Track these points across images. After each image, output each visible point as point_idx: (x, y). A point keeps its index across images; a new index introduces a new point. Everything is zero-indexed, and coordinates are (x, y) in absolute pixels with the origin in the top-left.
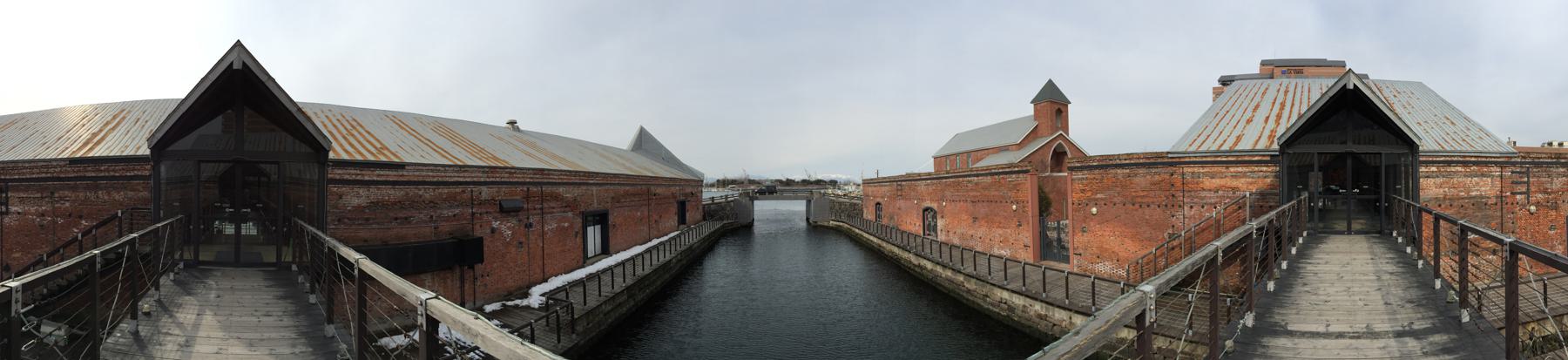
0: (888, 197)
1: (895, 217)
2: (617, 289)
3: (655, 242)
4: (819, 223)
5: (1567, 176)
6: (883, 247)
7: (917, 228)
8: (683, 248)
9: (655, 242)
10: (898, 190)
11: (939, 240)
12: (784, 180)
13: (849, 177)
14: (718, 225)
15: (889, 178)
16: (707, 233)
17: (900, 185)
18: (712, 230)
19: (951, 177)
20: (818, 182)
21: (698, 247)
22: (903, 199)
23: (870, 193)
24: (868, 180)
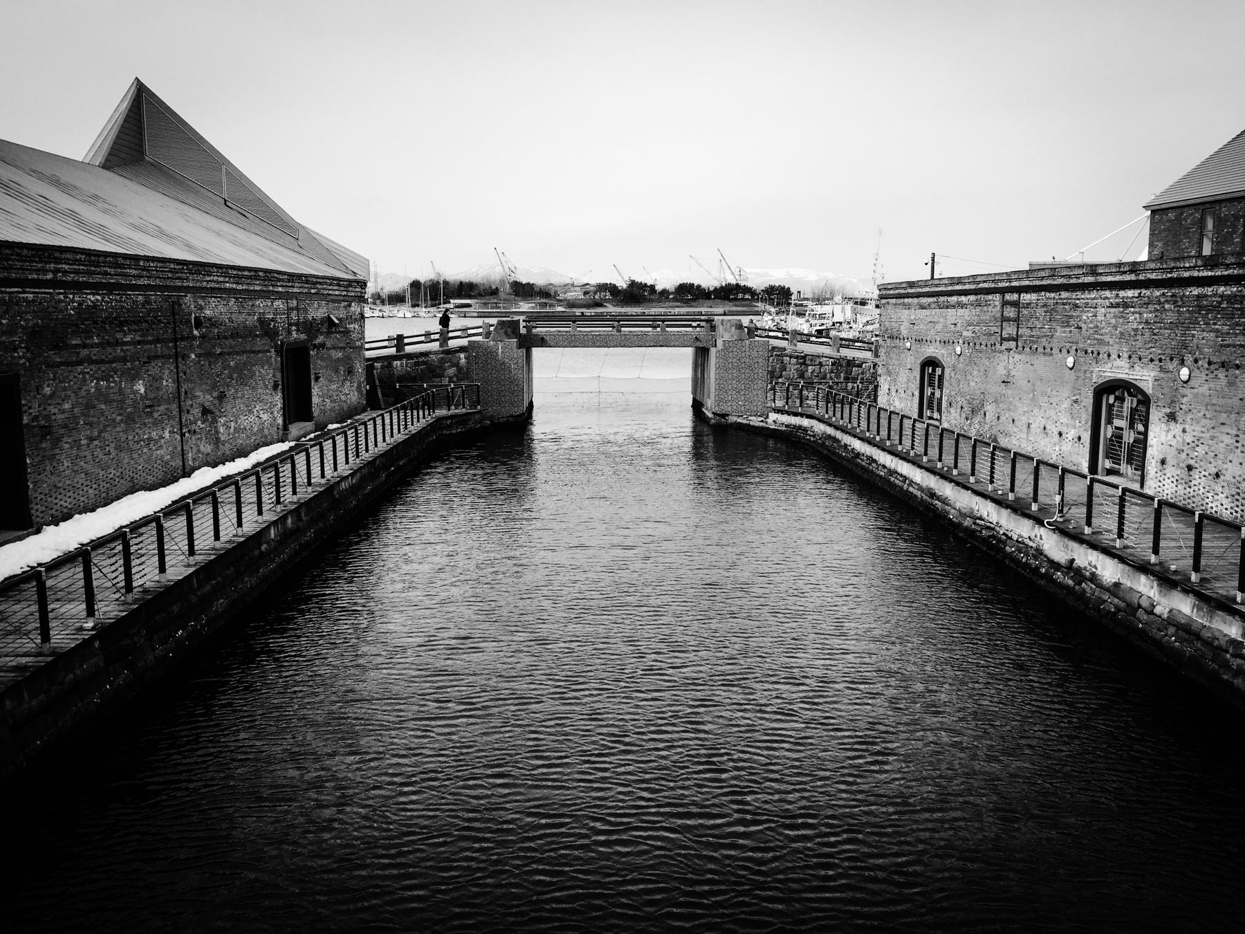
0: (967, 342)
1: (990, 408)
3: (205, 477)
4: (732, 419)
5: (1244, 335)
6: (944, 501)
8: (305, 493)
9: (205, 477)
10: (1004, 319)
11: (1148, 491)
12: (622, 284)
13: (830, 275)
14: (419, 422)
16: (382, 447)
17: (1015, 304)
18: (399, 437)
20: (730, 293)
21: (354, 489)
23: (904, 332)
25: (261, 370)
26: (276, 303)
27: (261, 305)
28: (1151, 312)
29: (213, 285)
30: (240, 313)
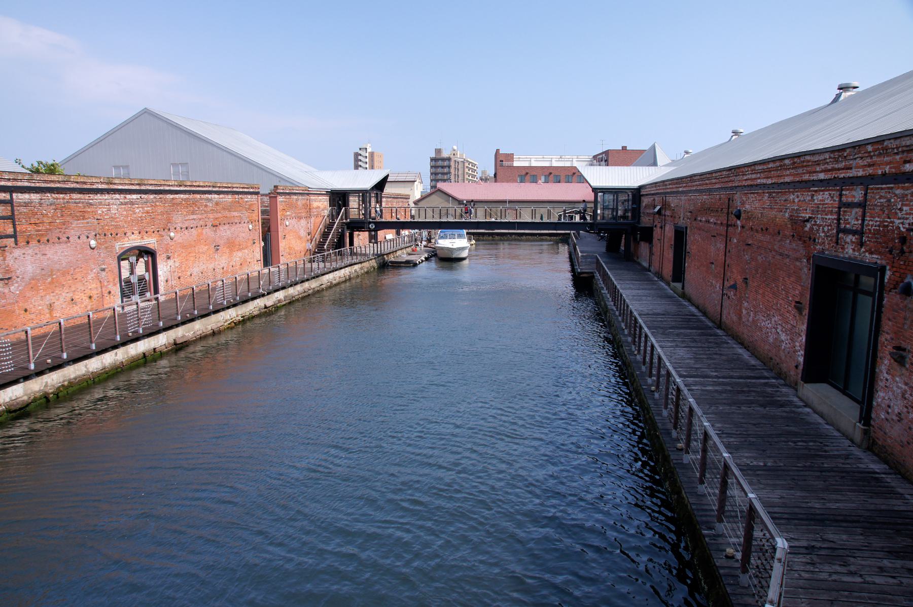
25: (786, 279)
26: (818, 197)
27: (796, 200)
28: (148, 207)
29: (749, 183)
30: (771, 208)
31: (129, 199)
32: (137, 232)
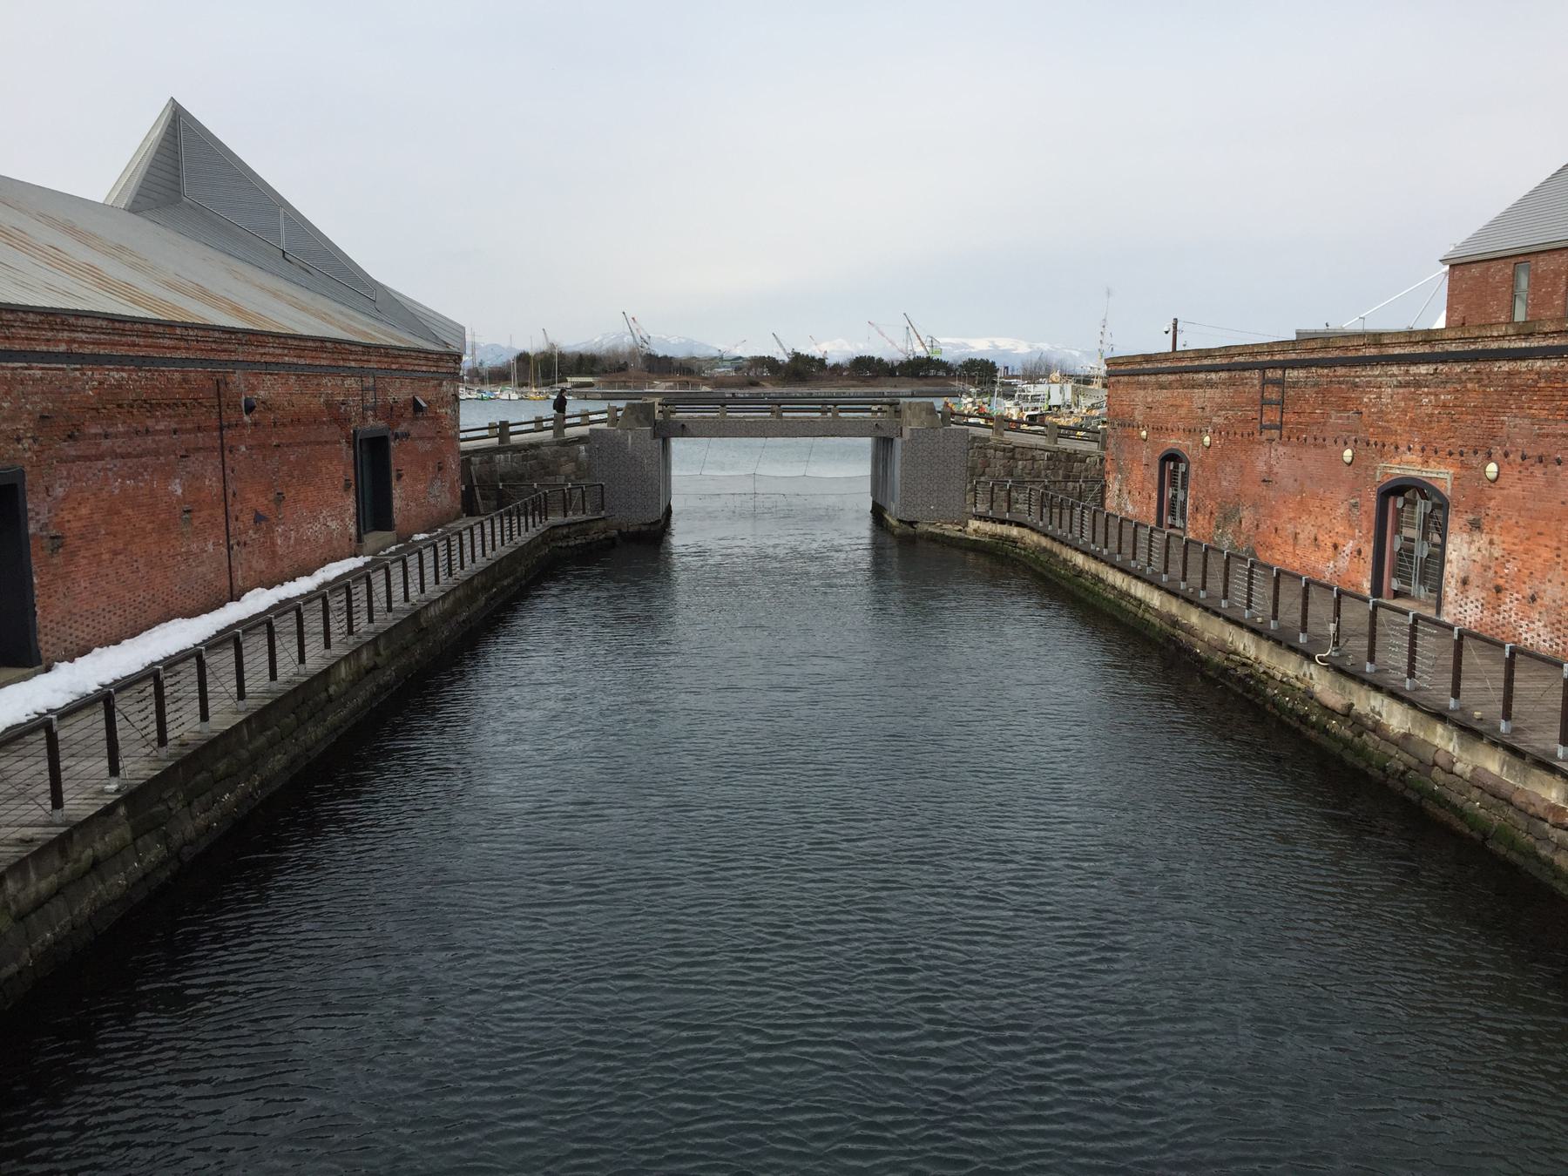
0: (1217, 431)
1: (1247, 515)
2: (78, 804)
3: (258, 601)
4: (923, 527)
6: (1190, 630)
7: (1343, 563)
8: (384, 621)
9: (258, 601)
14: (527, 532)
15: (1227, 351)
17: (1279, 383)
18: (503, 551)
19: (1544, 353)
20: (922, 370)
21: (446, 616)
22: (1285, 441)
24: (1130, 360)
26: (348, 382)
27: (329, 384)
29: (268, 359)
30: (302, 394)
31: (1414, 375)
32: (1418, 447)
